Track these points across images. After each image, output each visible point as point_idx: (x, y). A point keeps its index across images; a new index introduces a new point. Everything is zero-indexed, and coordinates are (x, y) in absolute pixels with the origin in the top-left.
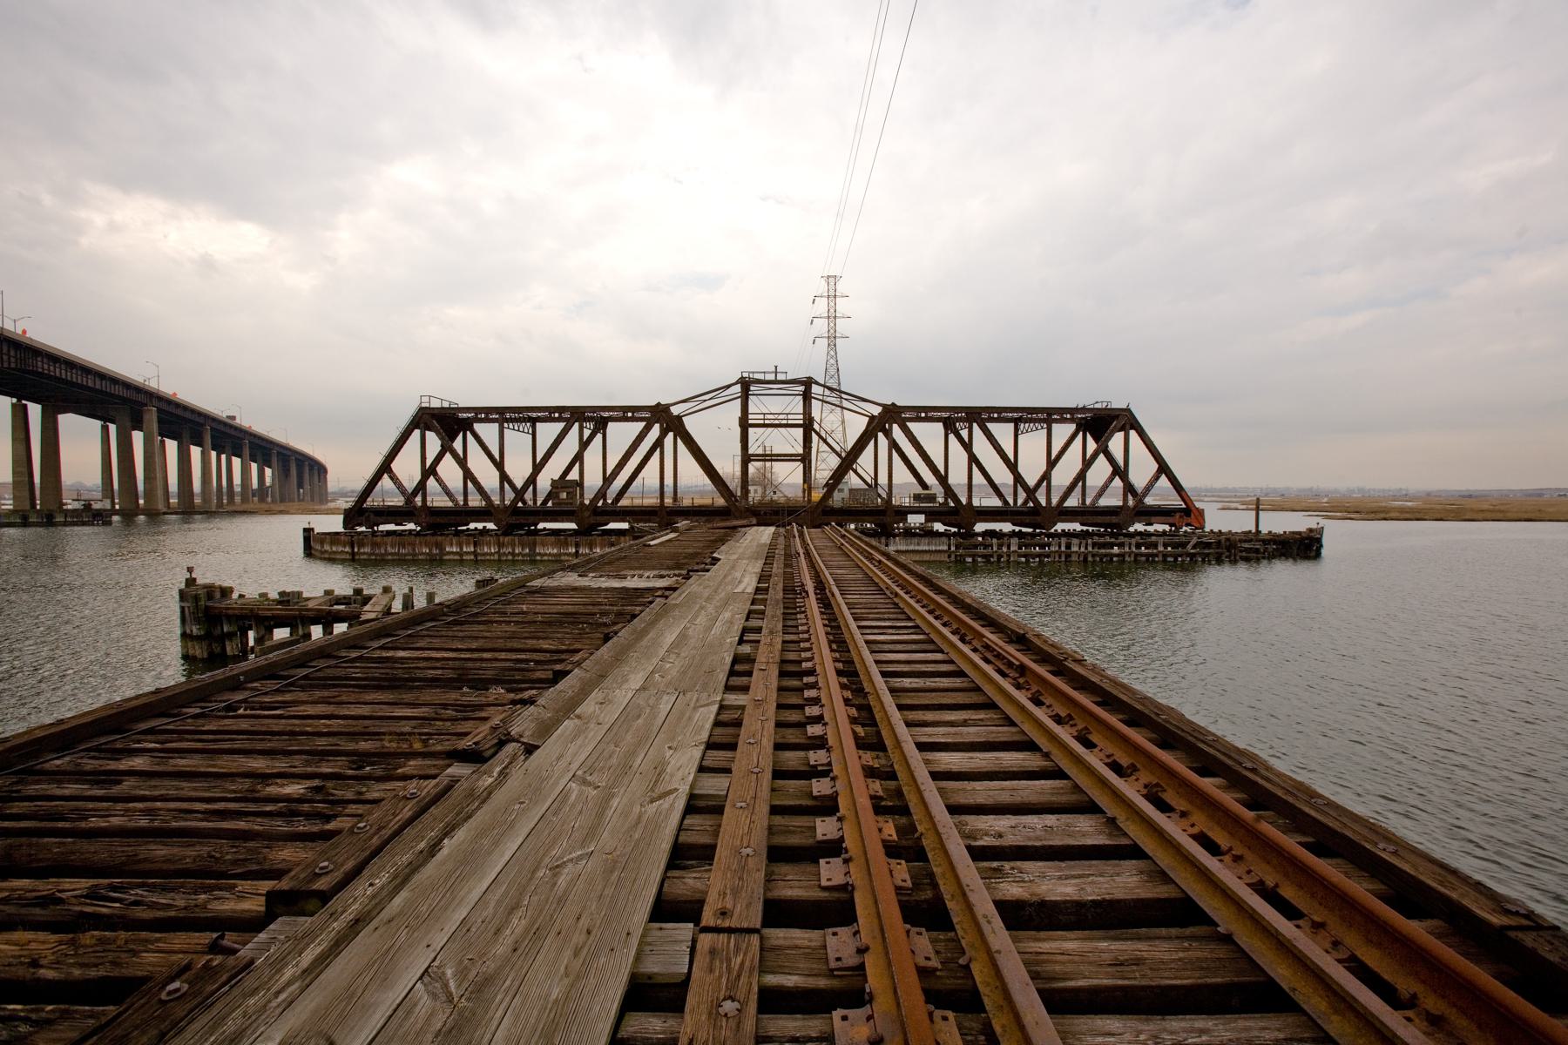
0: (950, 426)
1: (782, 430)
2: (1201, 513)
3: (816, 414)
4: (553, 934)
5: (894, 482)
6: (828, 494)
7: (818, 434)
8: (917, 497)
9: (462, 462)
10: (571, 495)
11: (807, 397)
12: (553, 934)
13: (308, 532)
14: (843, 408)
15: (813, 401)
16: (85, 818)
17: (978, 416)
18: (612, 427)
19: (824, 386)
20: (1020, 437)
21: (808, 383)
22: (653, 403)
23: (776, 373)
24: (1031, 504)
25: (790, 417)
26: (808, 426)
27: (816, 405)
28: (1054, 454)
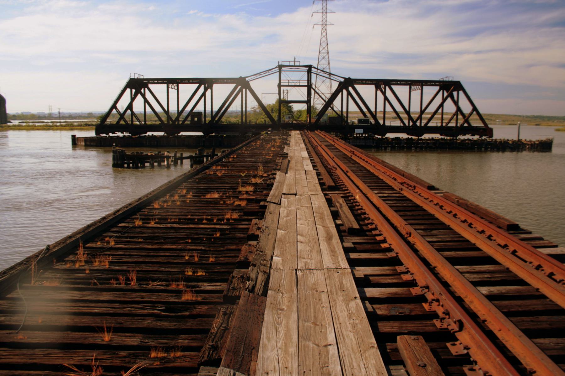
0: (378, 87)
1: (296, 88)
2: (491, 130)
3: (313, 81)
4: (210, 374)
5: (206, 110)
6: (318, 120)
7: (314, 90)
8: (360, 121)
9: (456, 103)
10: (199, 119)
11: (309, 72)
12: (210, 374)
13: (74, 137)
14: (331, 79)
15: (312, 74)
16: (130, 354)
17: (389, 83)
18: (216, 86)
19: (317, 69)
20: (412, 93)
21: (310, 67)
22: (238, 77)
23: (295, 61)
24: (466, 125)
25: (301, 82)
26: (309, 87)
27: (313, 76)
28: (203, 98)
